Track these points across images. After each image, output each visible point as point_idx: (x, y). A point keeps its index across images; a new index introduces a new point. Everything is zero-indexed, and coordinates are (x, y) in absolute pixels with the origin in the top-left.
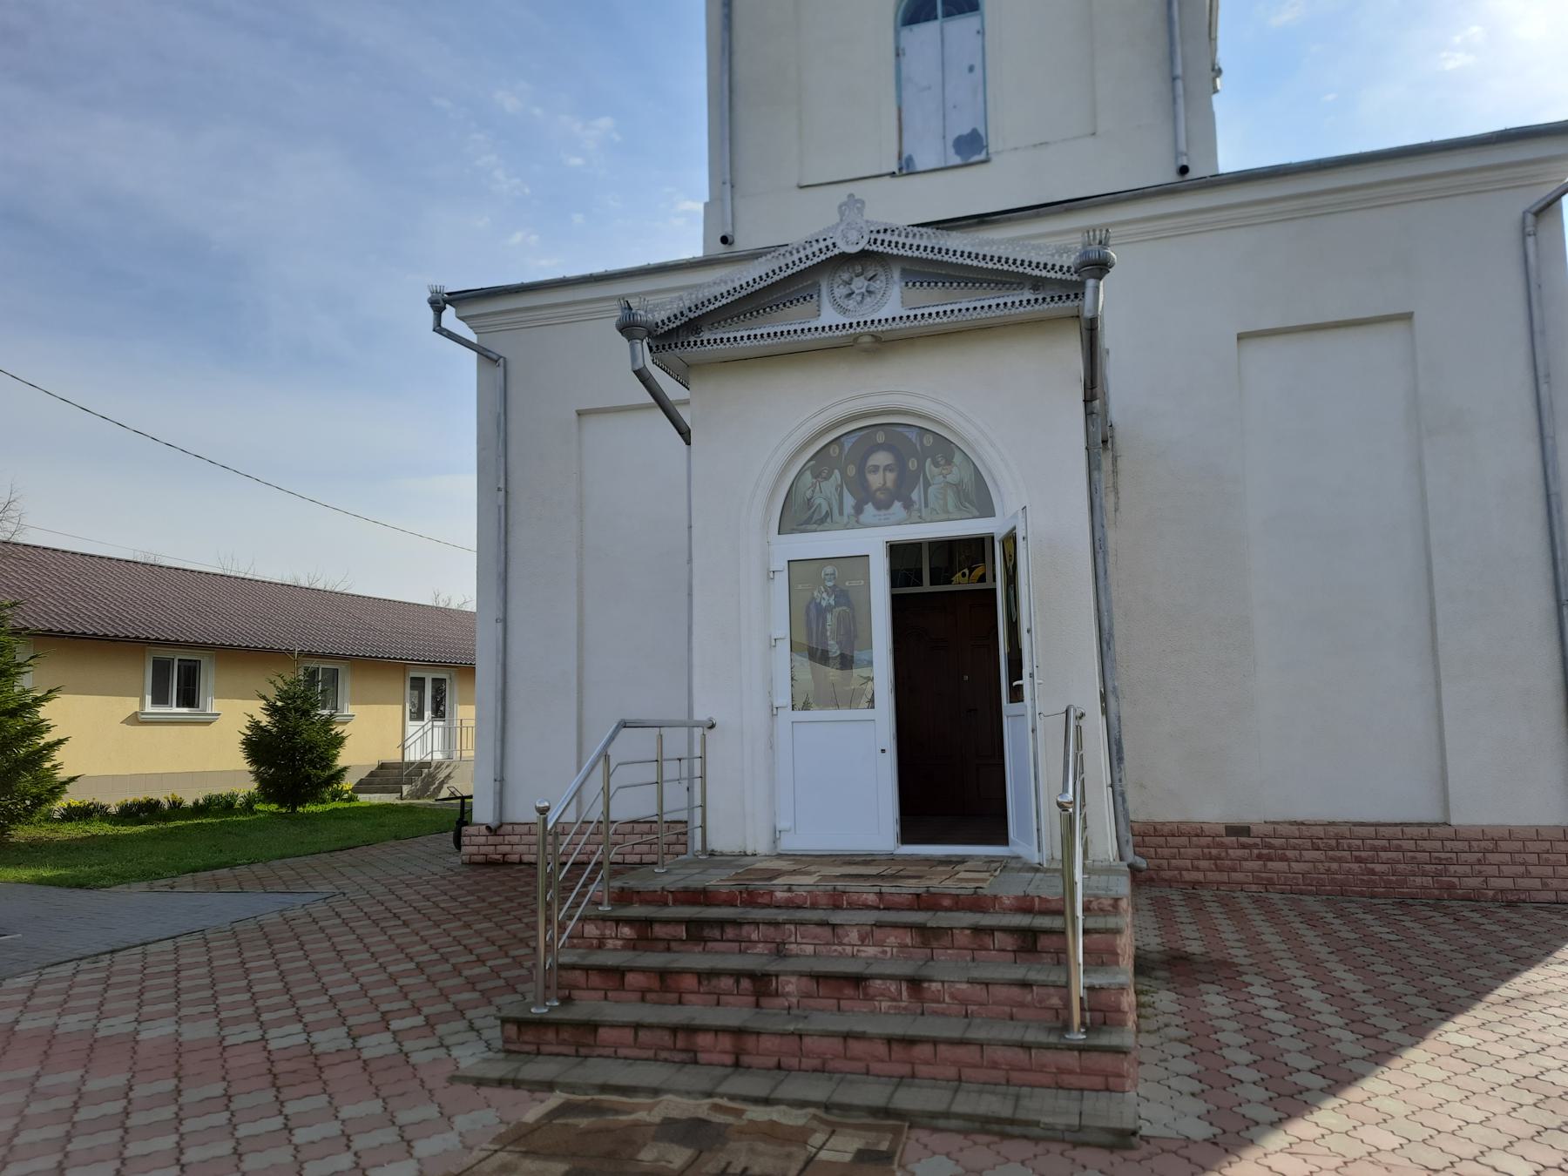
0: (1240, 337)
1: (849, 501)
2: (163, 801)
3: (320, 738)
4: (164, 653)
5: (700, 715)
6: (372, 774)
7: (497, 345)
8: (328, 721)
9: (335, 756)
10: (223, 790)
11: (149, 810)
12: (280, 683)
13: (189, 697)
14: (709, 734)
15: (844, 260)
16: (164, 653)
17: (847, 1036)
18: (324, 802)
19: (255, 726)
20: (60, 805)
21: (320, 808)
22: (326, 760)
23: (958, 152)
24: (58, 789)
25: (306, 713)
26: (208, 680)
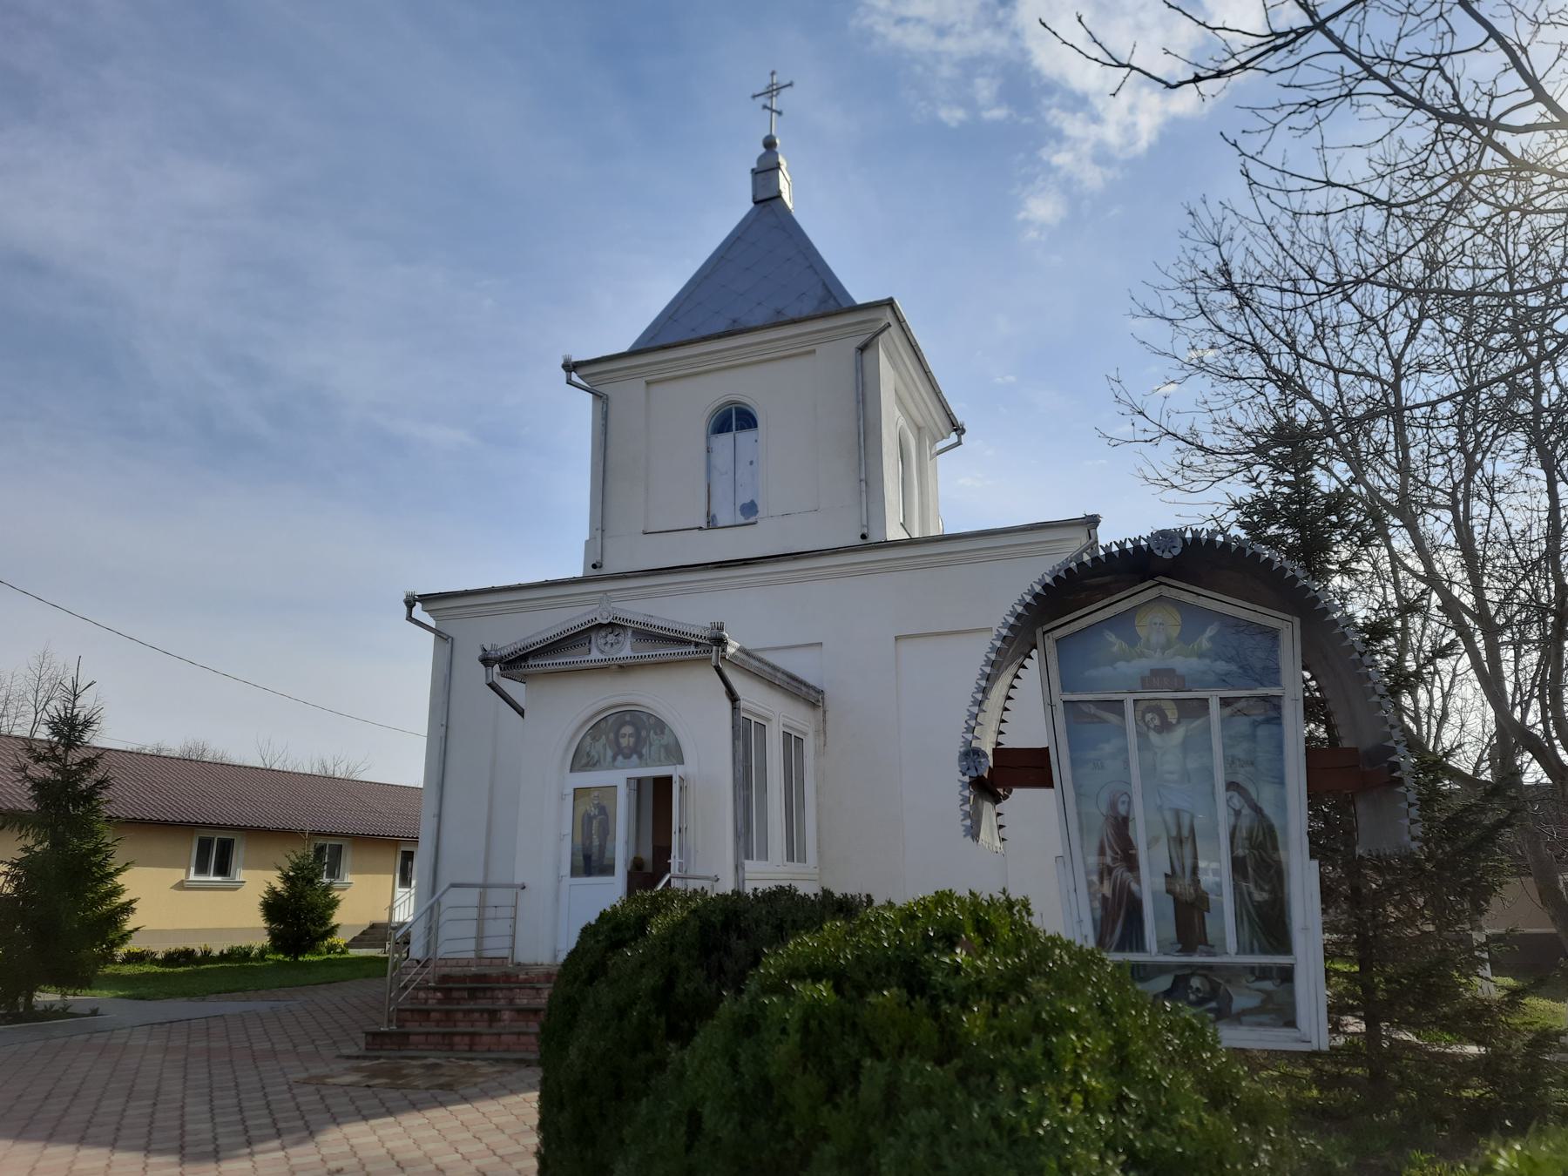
0: (897, 638)
1: (610, 753)
2: (197, 950)
3: (322, 901)
4: (206, 834)
5: (518, 881)
6: (364, 933)
7: (450, 628)
8: (328, 888)
9: (331, 916)
10: (244, 943)
11: (186, 956)
12: (293, 857)
13: (223, 869)
14: (521, 892)
15: (600, 626)
16: (206, 834)
17: (519, 1034)
18: (320, 954)
19: (272, 891)
20: (121, 952)
21: (316, 958)
22: (324, 918)
23: (743, 513)
24: (125, 937)
25: (311, 881)
26: (238, 854)
